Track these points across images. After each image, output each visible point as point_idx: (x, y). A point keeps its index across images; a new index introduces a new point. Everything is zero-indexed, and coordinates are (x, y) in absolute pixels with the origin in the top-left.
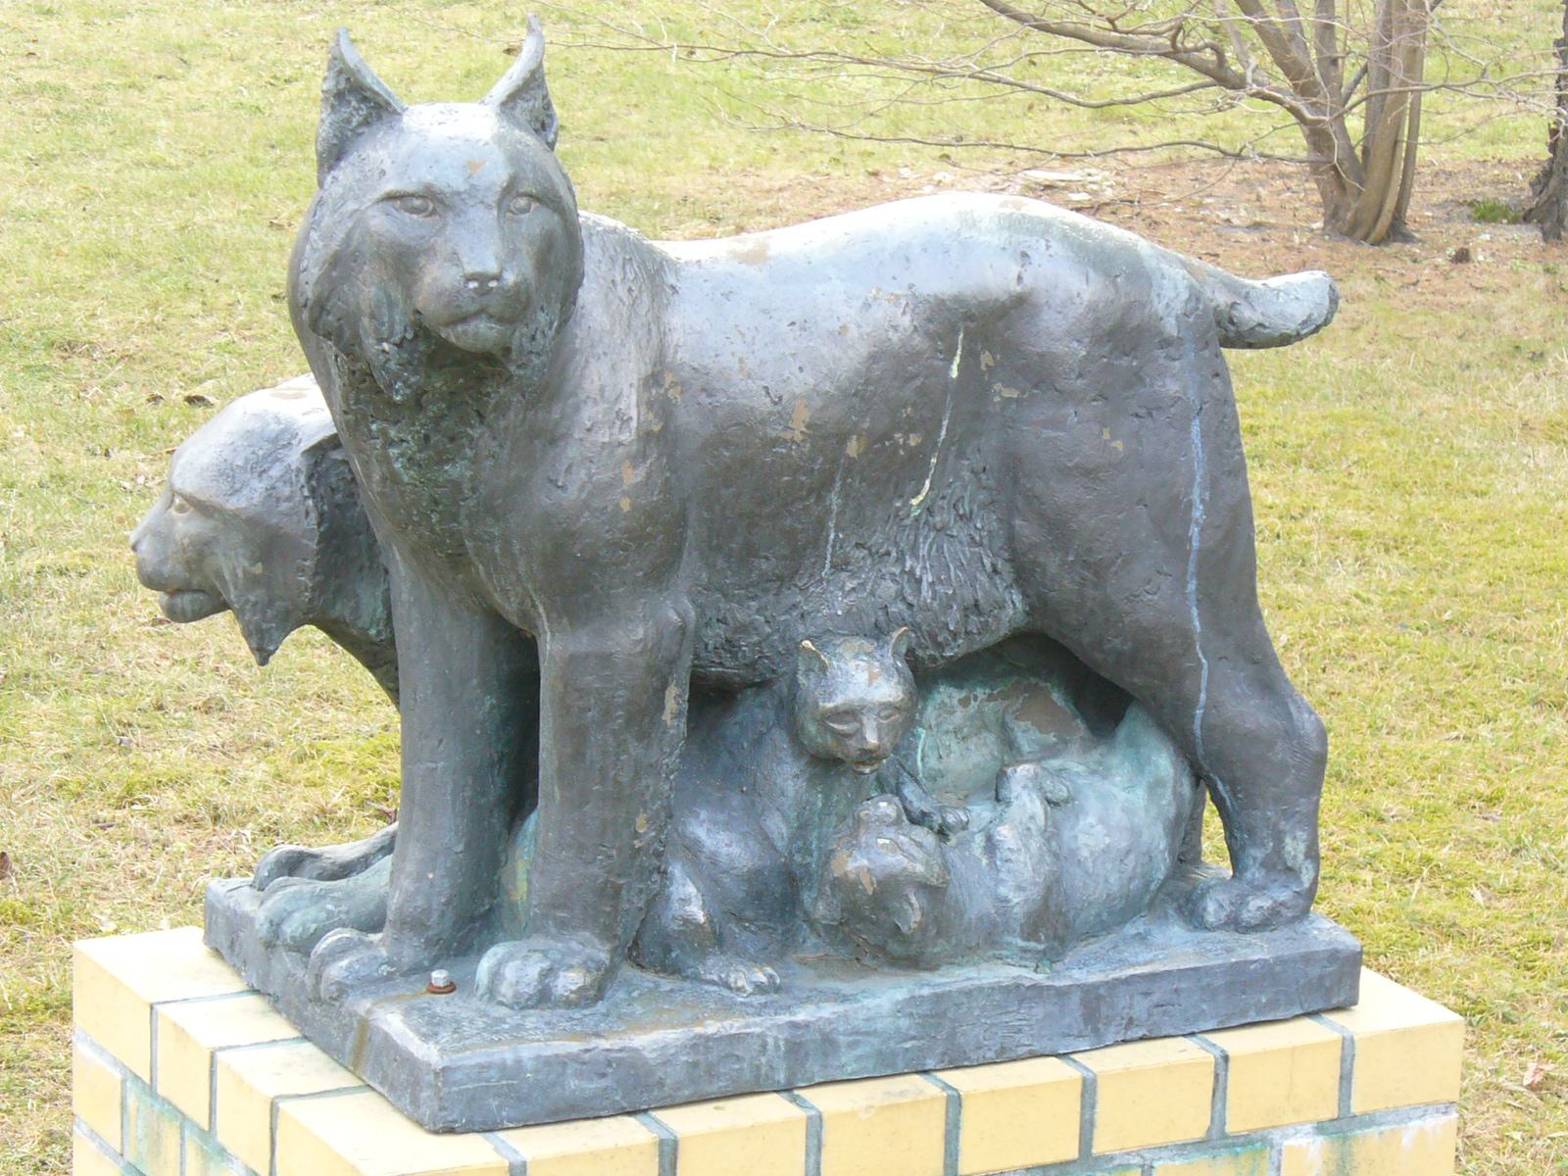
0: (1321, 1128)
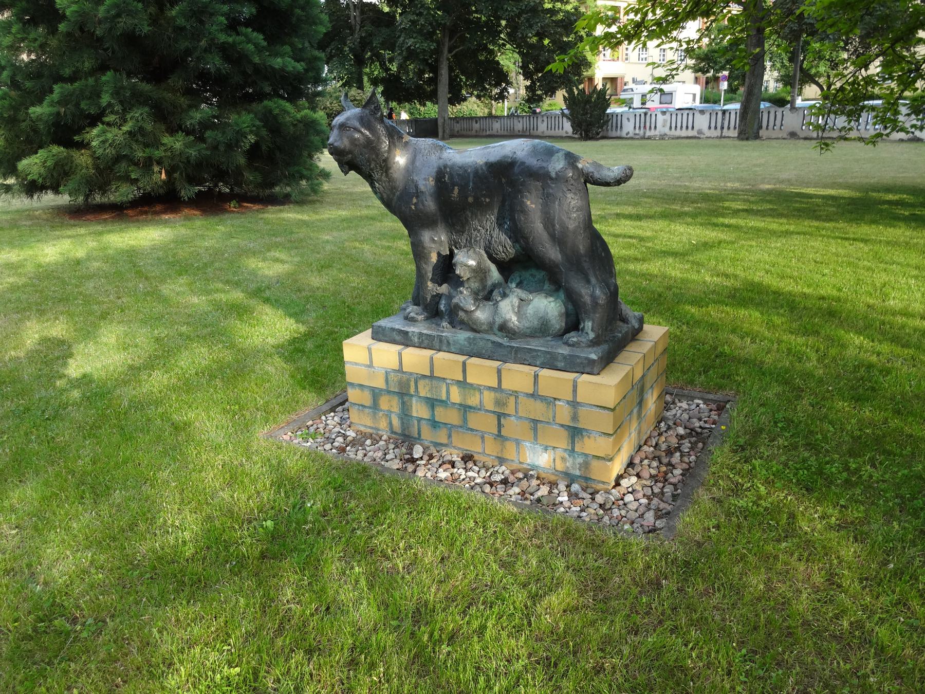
0: (568, 402)
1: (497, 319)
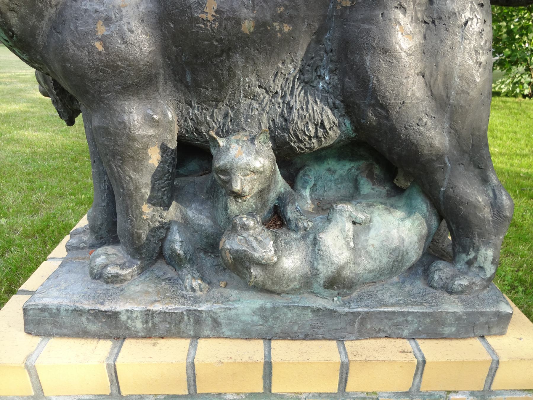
1: (321, 268)
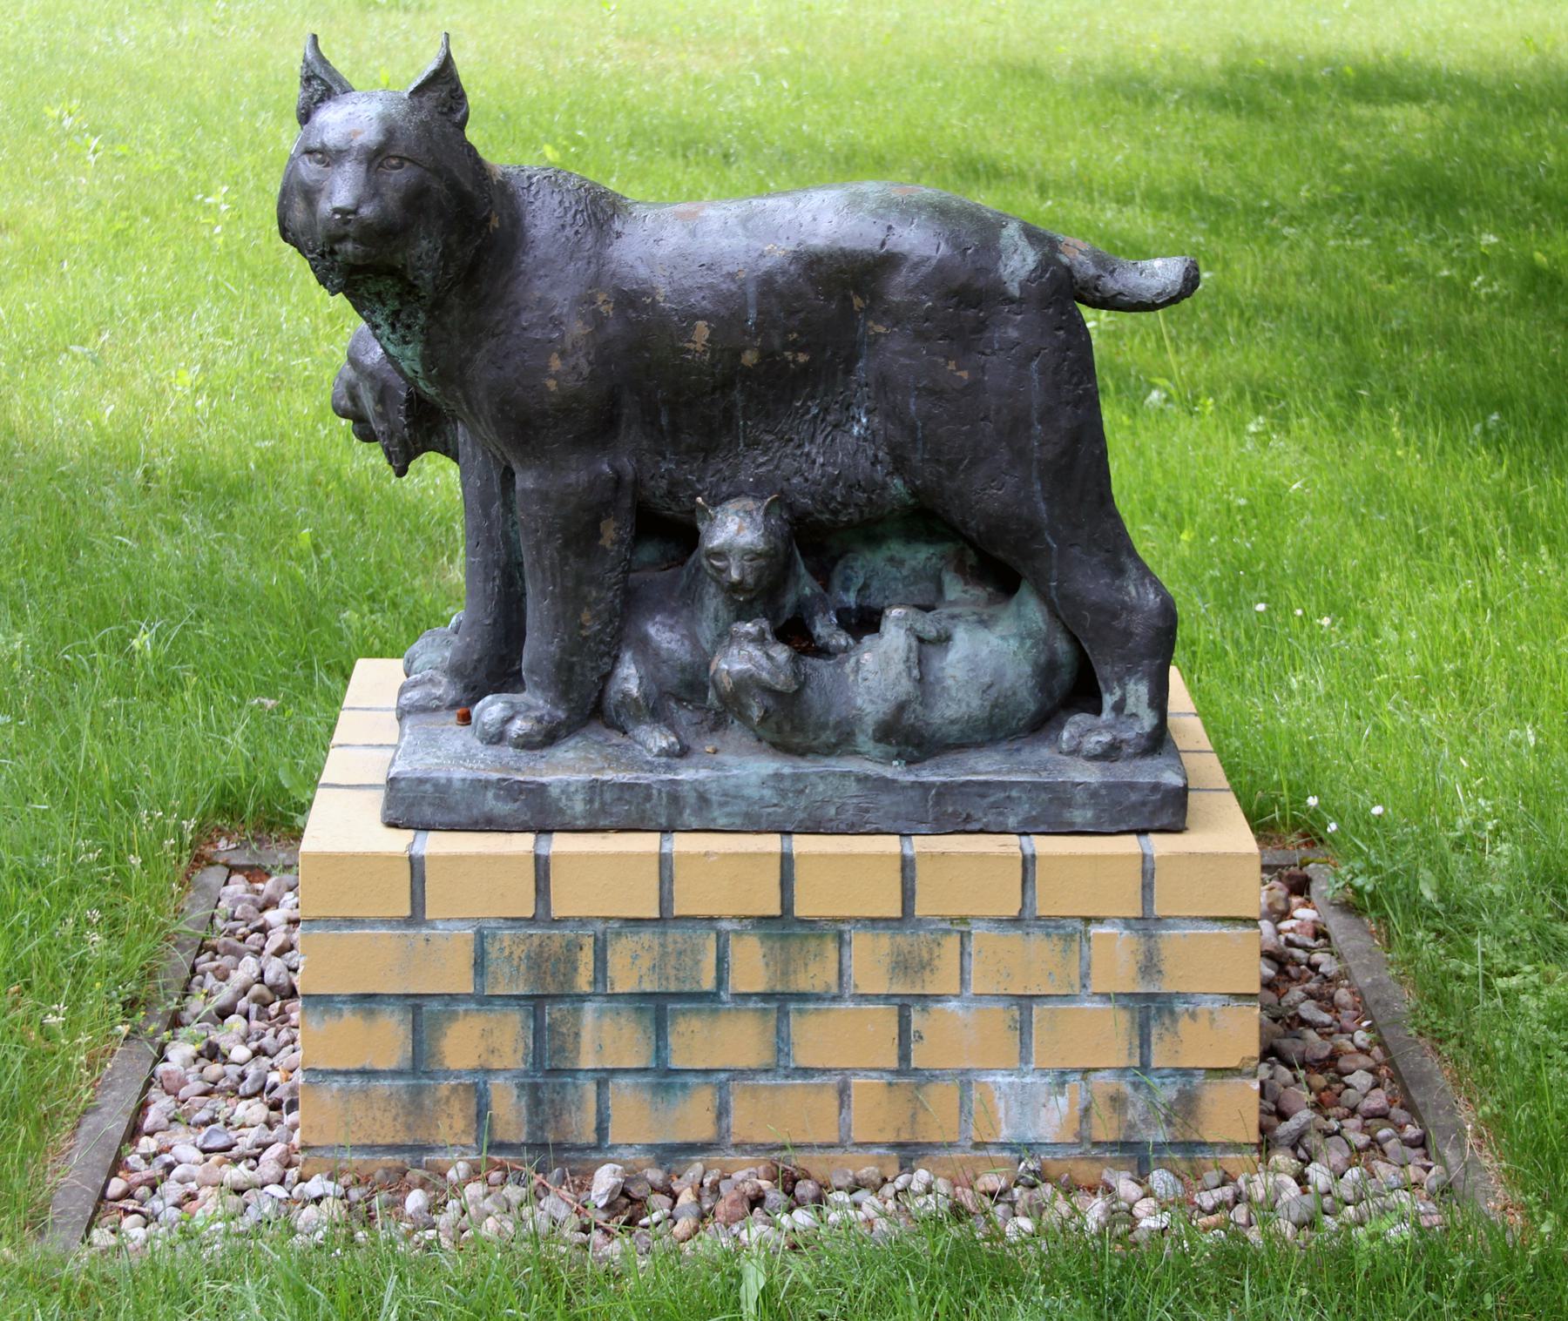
0: (1127, 922)
